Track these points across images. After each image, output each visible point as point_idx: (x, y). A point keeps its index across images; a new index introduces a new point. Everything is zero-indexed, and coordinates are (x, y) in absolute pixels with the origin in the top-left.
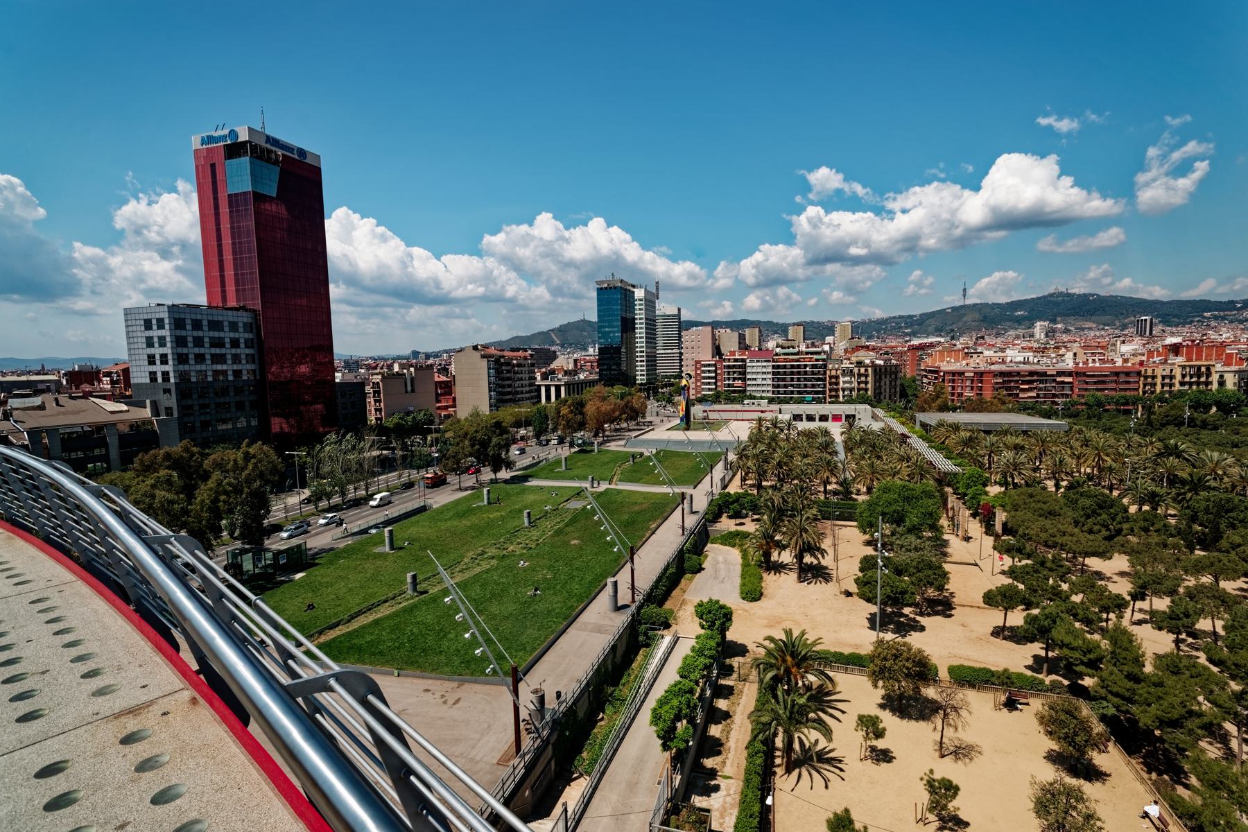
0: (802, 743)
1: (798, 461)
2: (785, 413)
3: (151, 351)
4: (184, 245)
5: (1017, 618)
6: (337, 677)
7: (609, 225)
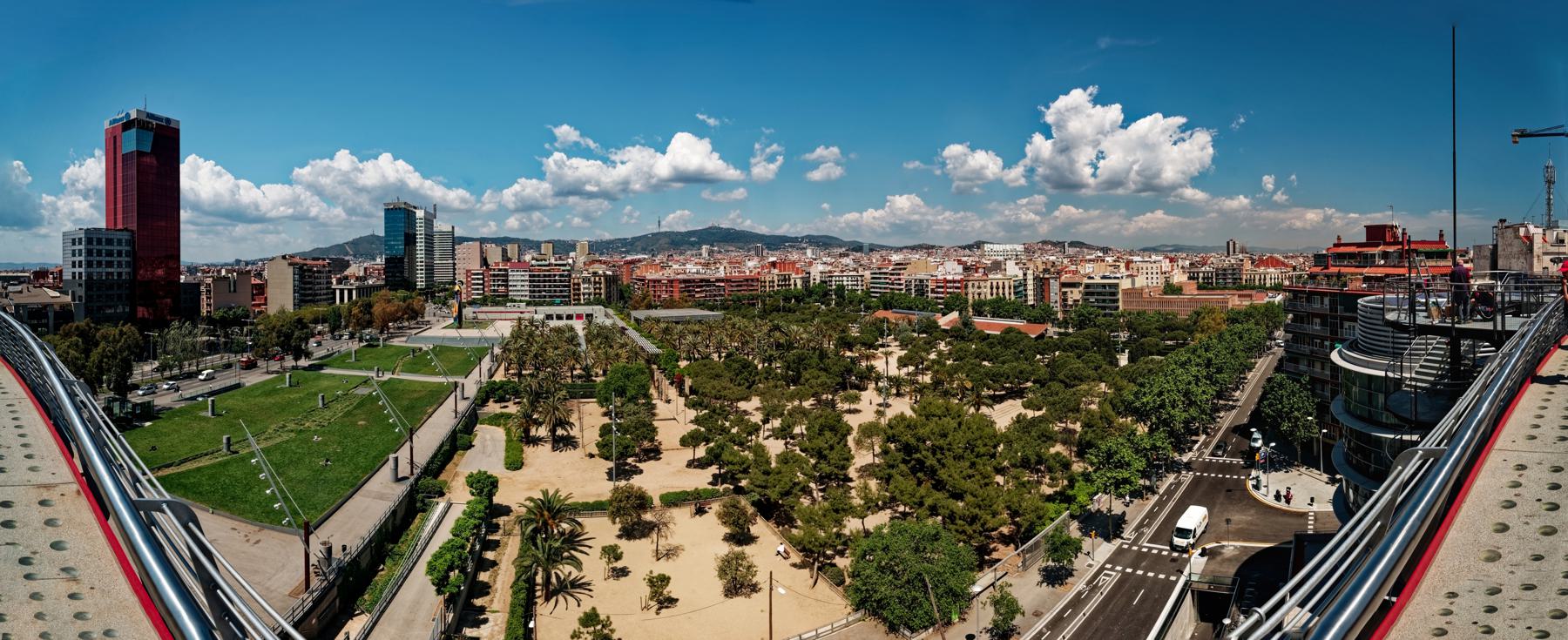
0: (558, 577)
1: (550, 352)
2: (540, 313)
4: (96, 190)
5: (701, 452)
6: (169, 503)
7: (395, 159)
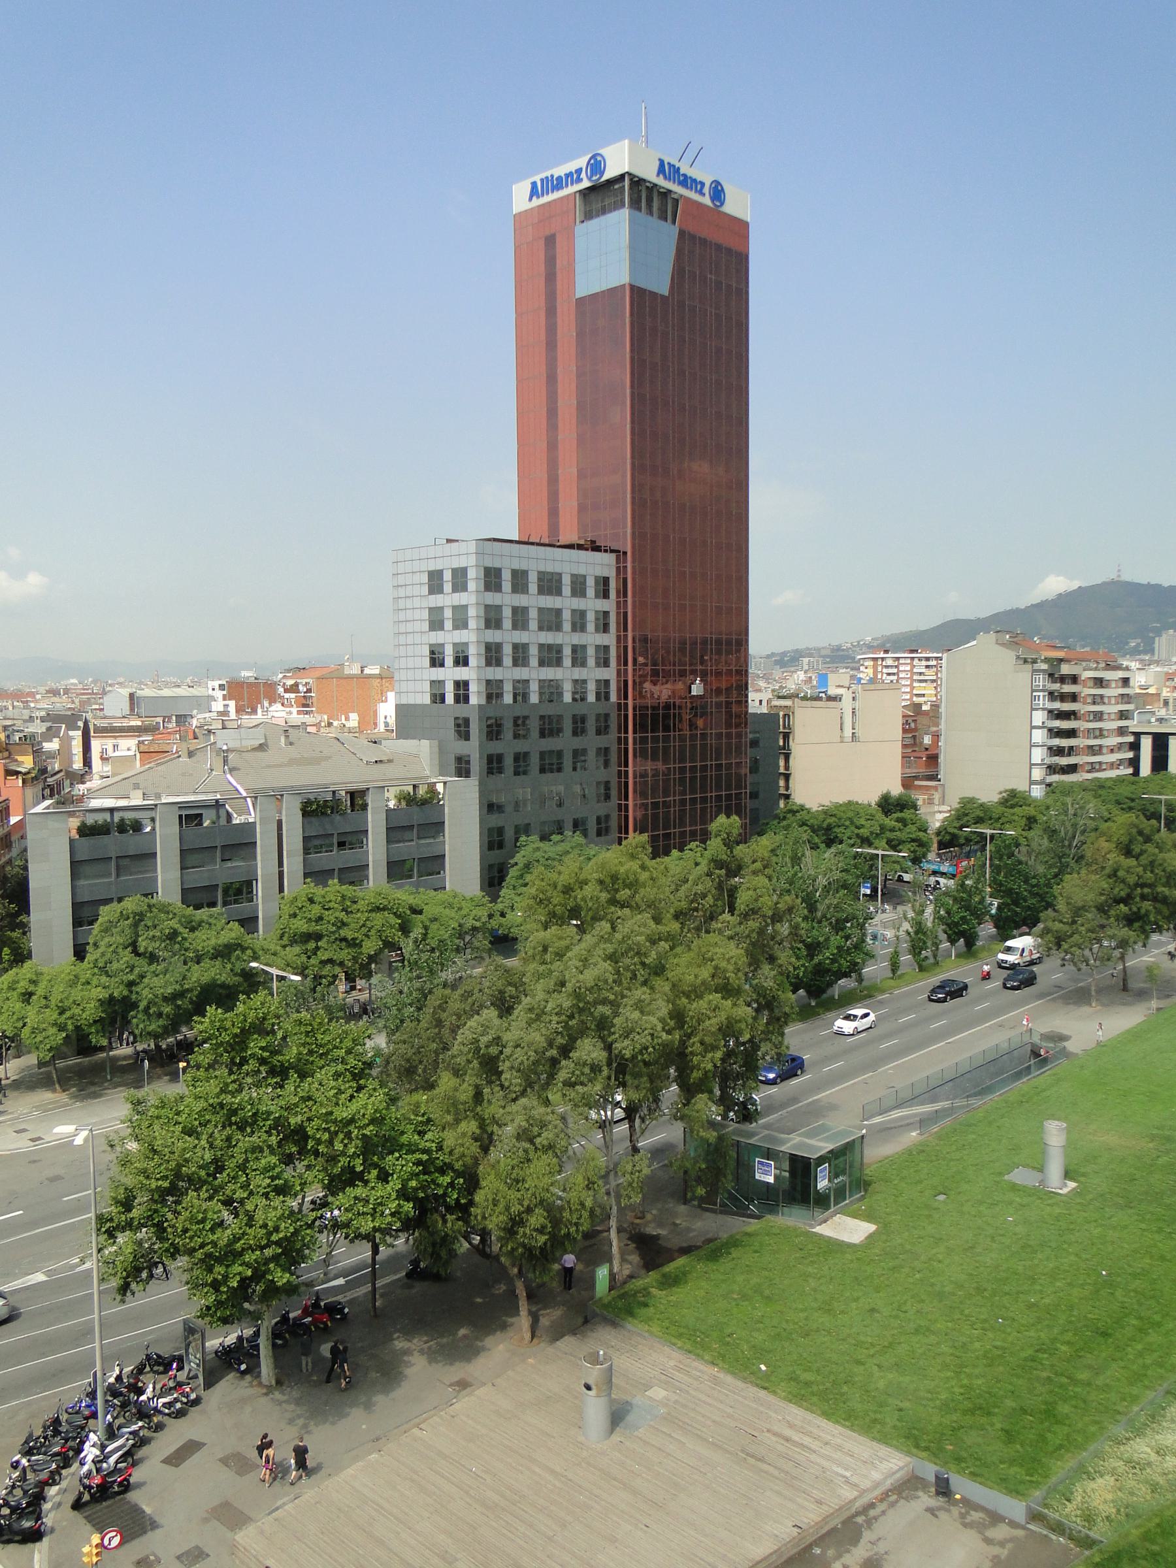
3: (437, 637)
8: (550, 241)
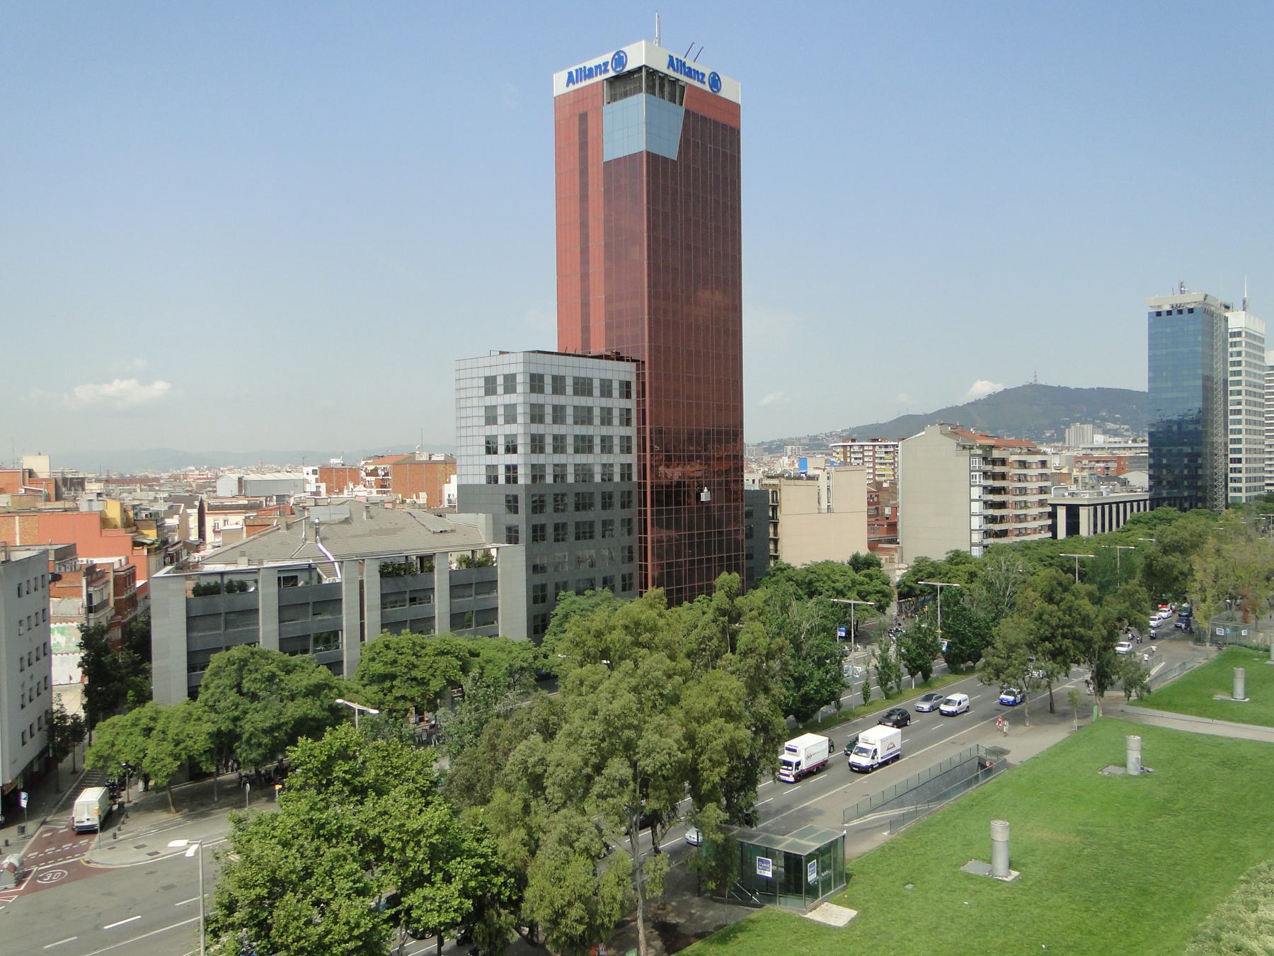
8: (583, 118)
